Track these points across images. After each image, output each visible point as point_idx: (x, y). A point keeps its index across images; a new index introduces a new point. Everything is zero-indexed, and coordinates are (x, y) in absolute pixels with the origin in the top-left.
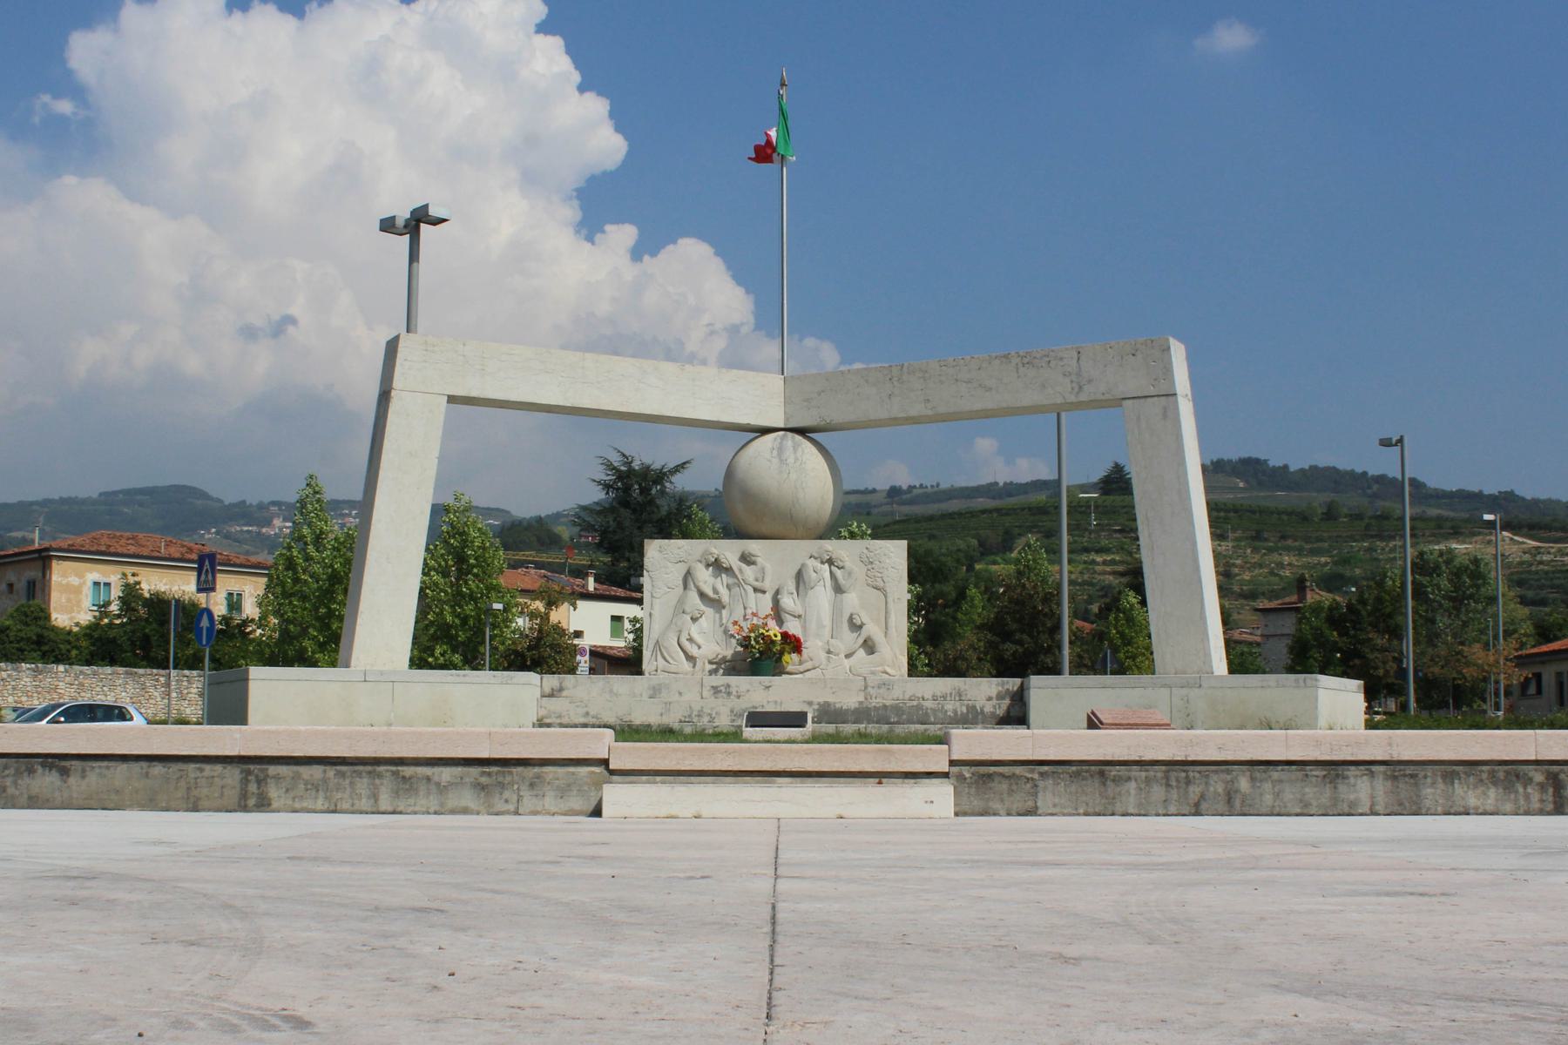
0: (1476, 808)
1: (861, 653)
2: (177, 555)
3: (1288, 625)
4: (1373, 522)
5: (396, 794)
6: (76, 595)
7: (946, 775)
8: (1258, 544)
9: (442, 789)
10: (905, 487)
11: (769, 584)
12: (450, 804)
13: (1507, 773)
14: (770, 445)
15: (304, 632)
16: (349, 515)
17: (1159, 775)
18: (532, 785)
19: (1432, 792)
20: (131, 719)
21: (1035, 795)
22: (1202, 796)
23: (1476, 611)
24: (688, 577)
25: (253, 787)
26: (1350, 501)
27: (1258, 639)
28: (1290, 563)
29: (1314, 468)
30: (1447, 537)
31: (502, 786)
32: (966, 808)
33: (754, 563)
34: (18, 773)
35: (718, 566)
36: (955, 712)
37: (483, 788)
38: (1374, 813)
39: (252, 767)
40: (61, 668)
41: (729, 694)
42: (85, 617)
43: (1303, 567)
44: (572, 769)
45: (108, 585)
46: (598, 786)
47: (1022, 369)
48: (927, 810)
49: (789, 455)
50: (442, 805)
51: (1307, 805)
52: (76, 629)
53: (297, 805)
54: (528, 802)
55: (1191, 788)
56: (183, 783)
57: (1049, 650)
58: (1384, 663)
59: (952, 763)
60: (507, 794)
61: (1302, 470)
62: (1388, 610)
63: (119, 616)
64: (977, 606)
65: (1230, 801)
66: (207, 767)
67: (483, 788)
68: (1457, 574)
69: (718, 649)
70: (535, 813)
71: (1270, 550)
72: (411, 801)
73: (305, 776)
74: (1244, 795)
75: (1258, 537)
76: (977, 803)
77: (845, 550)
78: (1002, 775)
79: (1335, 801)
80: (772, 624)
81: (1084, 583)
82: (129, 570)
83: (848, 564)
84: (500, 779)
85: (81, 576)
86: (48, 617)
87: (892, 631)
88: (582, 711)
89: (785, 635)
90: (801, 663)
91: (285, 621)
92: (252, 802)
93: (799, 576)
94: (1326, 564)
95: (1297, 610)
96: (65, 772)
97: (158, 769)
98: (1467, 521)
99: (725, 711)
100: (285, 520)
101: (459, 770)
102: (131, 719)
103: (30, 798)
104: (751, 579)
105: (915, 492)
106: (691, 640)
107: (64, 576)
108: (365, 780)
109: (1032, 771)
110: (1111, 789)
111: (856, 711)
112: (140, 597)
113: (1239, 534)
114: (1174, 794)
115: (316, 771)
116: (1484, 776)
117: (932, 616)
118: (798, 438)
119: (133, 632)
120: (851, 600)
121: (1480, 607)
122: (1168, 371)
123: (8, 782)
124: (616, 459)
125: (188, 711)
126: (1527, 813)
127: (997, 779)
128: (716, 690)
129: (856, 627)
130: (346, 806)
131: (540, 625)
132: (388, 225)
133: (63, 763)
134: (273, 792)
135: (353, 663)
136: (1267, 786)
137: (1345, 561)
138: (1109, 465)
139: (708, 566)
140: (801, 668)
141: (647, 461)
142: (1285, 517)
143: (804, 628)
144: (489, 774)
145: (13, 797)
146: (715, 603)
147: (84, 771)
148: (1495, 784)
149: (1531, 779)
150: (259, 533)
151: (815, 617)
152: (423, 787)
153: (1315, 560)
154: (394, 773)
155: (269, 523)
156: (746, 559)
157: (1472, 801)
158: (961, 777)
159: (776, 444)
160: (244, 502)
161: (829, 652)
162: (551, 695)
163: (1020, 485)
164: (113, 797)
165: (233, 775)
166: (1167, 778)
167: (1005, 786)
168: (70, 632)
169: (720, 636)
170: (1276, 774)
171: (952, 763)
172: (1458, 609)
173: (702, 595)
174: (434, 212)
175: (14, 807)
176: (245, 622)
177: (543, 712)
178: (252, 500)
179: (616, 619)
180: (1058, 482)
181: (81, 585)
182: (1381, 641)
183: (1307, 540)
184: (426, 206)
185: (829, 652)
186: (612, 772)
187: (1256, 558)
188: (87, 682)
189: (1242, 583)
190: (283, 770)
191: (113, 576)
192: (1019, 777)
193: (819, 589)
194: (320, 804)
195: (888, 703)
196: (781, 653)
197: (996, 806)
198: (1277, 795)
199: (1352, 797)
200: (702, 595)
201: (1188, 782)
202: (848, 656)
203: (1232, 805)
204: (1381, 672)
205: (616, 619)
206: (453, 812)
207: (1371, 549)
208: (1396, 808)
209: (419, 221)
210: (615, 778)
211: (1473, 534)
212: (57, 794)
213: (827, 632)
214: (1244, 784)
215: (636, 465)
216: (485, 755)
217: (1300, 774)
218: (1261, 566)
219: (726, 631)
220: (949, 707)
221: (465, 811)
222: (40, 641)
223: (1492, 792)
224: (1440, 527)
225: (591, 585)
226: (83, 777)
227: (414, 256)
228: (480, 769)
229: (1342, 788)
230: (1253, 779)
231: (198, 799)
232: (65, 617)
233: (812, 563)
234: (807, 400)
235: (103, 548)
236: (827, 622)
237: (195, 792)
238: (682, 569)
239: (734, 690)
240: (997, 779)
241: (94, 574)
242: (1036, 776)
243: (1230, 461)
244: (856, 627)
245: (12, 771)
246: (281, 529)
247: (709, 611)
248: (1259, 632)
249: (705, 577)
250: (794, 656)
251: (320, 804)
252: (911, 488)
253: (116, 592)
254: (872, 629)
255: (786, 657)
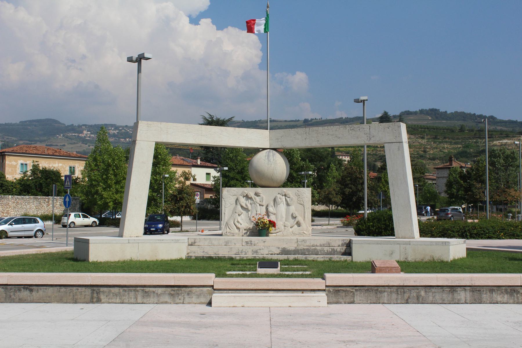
0: (500, 301)
1: (296, 226)
2: (51, 154)
3: (446, 173)
4: (477, 132)
5: (143, 297)
6: (15, 169)
7: (324, 290)
8: (436, 140)
9: (158, 295)
10: (310, 119)
11: (264, 203)
12: (161, 300)
13: (511, 290)
14: (265, 154)
15: (99, 185)
16: (111, 129)
17: (395, 290)
18: (188, 294)
19: (485, 296)
20: (38, 223)
21: (354, 297)
22: (409, 297)
23: (512, 171)
24: (237, 200)
25: (95, 295)
26: (469, 124)
27: (435, 178)
28: (448, 148)
29: (456, 112)
30: (504, 138)
31: (178, 294)
32: (331, 301)
33: (259, 196)
34: (15, 291)
35: (247, 197)
36: (328, 251)
37: (172, 295)
38: (466, 303)
39: (95, 288)
40: (10, 196)
41: (251, 244)
42: (19, 176)
43: (452, 149)
44: (201, 289)
45: (26, 164)
46: (211, 294)
47: (350, 131)
48: (317, 304)
49: (271, 158)
50: (158, 301)
51: (444, 300)
52: (15, 181)
53: (110, 301)
54: (187, 299)
55: (405, 295)
56: (71, 294)
57: (360, 191)
58: (479, 193)
59: (326, 286)
60: (180, 297)
61: (452, 113)
62: (481, 174)
63: (31, 176)
64: (334, 173)
65: (418, 298)
66: (80, 288)
67: (172, 295)
68: (507, 158)
69: (247, 225)
70: (189, 303)
71: (440, 143)
72: (148, 299)
73: (113, 291)
74: (423, 297)
75: (436, 138)
76: (335, 300)
77: (291, 191)
78: (343, 290)
79: (453, 299)
80: (266, 217)
81: (373, 154)
82: (35, 159)
83: (291, 196)
84: (178, 292)
85: (16, 161)
86: (5, 177)
87: (306, 219)
88: (202, 251)
89: (270, 221)
90: (275, 230)
91: (91, 180)
92: (95, 300)
93: (275, 200)
94: (460, 147)
95: (449, 168)
96: (31, 291)
97: (63, 289)
98: (511, 132)
99: (250, 251)
100: (88, 131)
101: (164, 289)
102: (38, 223)
103: (19, 299)
104: (258, 202)
105: (313, 121)
106: (238, 222)
107: (10, 162)
108: (133, 293)
109: (353, 289)
110: (379, 295)
111: (294, 250)
112: (38, 169)
113: (429, 137)
114: (400, 297)
115: (116, 290)
116: (503, 291)
117: (320, 174)
118: (274, 152)
119: (36, 182)
120: (292, 209)
121: (514, 169)
122: (400, 134)
123: (12, 294)
124: (207, 116)
125: (56, 211)
126: (517, 303)
127: (341, 292)
128: (247, 243)
129: (294, 218)
130: (126, 301)
131: (183, 186)
132: (130, 60)
133: (31, 287)
134: (102, 297)
135: (124, 234)
136: (430, 294)
137: (467, 147)
138: (383, 112)
139: (244, 197)
140: (276, 232)
141: (219, 117)
142: (445, 131)
143: (277, 218)
144: (174, 290)
145: (13, 299)
146: (246, 210)
147: (38, 290)
148: (507, 293)
149: (519, 292)
150: (78, 136)
151: (280, 214)
152: (152, 295)
153: (456, 146)
154: (142, 290)
155: (82, 132)
156: (257, 194)
157: (499, 299)
158: (329, 291)
159: (267, 155)
160: (73, 125)
161: (285, 226)
162: (191, 245)
163: (350, 119)
164: (48, 299)
165: (88, 291)
166: (397, 291)
167: (344, 294)
168: (13, 182)
169: (248, 221)
170: (433, 290)
171: (326, 286)
172: (506, 170)
173: (242, 207)
174: (146, 55)
175: (14, 302)
176: (77, 179)
177: (189, 251)
178: (76, 124)
179: (208, 174)
180: (363, 117)
181: (16, 165)
182: (479, 185)
183: (453, 139)
184: (144, 53)
185: (285, 226)
186: (215, 290)
187: (435, 145)
188: (20, 201)
189: (430, 154)
190: (105, 289)
191: (30, 162)
192: (348, 291)
193: (282, 205)
194: (118, 300)
195: (305, 248)
196: (269, 227)
197: (341, 300)
198: (434, 297)
199: (459, 297)
200: (242, 207)
201: (404, 292)
202: (291, 227)
203: (419, 300)
204: (478, 197)
205: (208, 174)
206: (162, 303)
207: (476, 142)
208: (474, 301)
209: (141, 59)
210: (215, 291)
211: (514, 137)
212: (29, 298)
213: (284, 219)
214: (423, 293)
215: (215, 119)
216: (173, 284)
217: (441, 290)
218: (437, 148)
219: (250, 219)
220: (326, 249)
221: (166, 303)
222: (2, 185)
223: (506, 296)
224: (501, 134)
225: (199, 162)
226: (38, 292)
227: (139, 70)
228: (171, 289)
229: (455, 295)
230: (426, 292)
231: (77, 299)
232: (11, 176)
233: (279, 196)
234: (277, 139)
235: (24, 152)
236: (284, 216)
237: (76, 297)
238: (235, 198)
239: (253, 243)
240: (341, 292)
241: (21, 160)
242: (354, 291)
243: (426, 110)
244: (294, 218)
245: (13, 290)
246: (86, 134)
247: (244, 212)
248: (435, 175)
249: (243, 201)
250: (273, 228)
251: (118, 300)
252: (312, 120)
253: (30, 168)
254: (300, 218)
255: (270, 229)
